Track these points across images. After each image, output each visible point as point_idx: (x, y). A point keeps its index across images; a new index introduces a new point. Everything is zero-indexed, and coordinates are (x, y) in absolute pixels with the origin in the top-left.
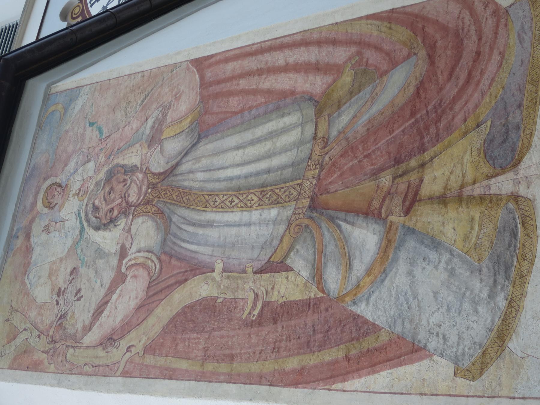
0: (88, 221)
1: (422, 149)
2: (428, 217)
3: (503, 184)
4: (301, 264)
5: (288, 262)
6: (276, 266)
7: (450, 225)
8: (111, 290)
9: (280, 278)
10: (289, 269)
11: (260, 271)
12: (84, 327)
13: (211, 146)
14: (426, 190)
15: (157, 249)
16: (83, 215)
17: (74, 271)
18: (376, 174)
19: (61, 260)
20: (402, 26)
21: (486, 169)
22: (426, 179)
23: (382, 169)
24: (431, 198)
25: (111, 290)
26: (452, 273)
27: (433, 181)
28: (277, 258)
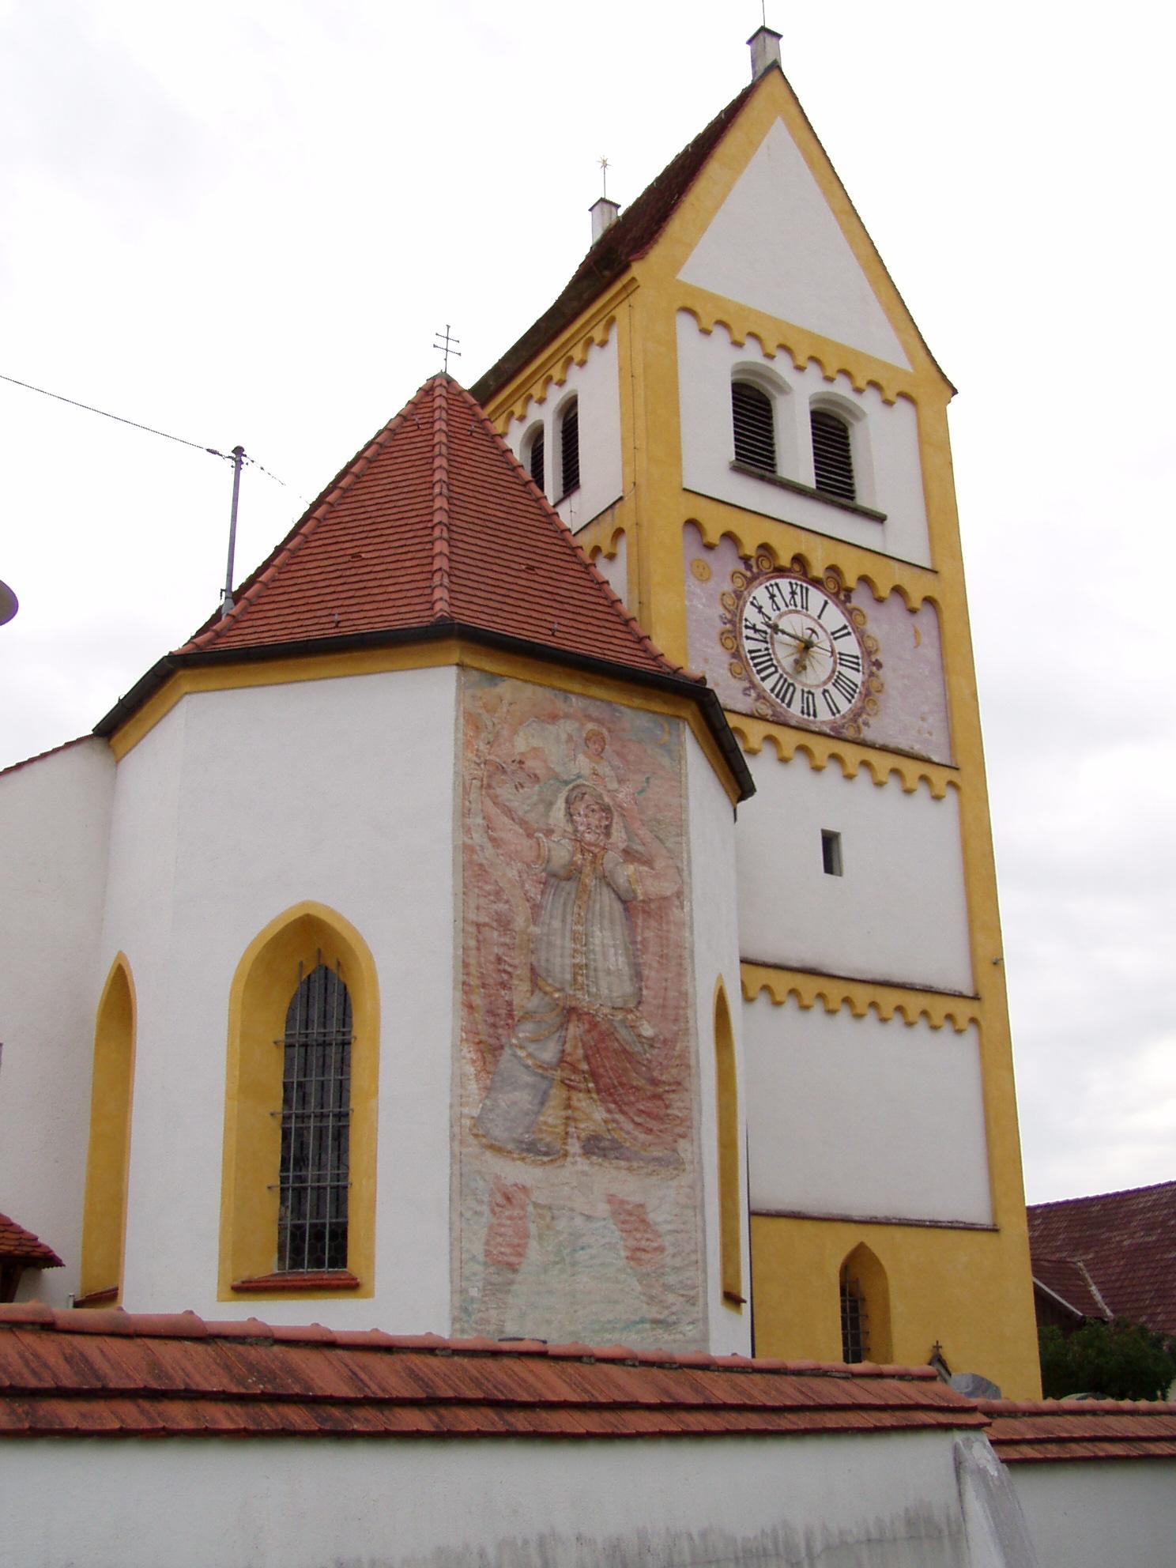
0: (573, 789)
1: (598, 1091)
2: (557, 1094)
3: (574, 1147)
4: (534, 1002)
5: (537, 992)
6: (535, 977)
7: (552, 1116)
8: (523, 823)
9: (525, 986)
10: (532, 992)
11: (533, 969)
12: (497, 796)
13: (617, 914)
14: (575, 1095)
15: (498, 439)
16: (579, 782)
17: (536, 778)
18: (587, 1058)
19: (545, 761)
20: (711, 691)
21: (583, 1135)
22: (581, 1095)
23: (589, 1064)
24: (569, 1099)
25: (523, 823)
26: (527, 1114)
27: (581, 1101)
28: (541, 983)
